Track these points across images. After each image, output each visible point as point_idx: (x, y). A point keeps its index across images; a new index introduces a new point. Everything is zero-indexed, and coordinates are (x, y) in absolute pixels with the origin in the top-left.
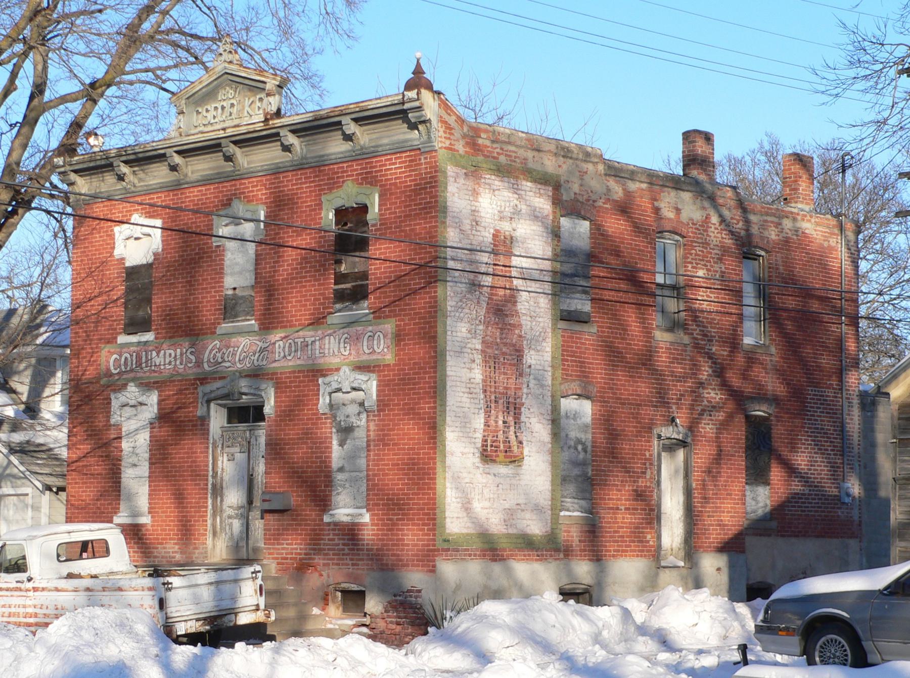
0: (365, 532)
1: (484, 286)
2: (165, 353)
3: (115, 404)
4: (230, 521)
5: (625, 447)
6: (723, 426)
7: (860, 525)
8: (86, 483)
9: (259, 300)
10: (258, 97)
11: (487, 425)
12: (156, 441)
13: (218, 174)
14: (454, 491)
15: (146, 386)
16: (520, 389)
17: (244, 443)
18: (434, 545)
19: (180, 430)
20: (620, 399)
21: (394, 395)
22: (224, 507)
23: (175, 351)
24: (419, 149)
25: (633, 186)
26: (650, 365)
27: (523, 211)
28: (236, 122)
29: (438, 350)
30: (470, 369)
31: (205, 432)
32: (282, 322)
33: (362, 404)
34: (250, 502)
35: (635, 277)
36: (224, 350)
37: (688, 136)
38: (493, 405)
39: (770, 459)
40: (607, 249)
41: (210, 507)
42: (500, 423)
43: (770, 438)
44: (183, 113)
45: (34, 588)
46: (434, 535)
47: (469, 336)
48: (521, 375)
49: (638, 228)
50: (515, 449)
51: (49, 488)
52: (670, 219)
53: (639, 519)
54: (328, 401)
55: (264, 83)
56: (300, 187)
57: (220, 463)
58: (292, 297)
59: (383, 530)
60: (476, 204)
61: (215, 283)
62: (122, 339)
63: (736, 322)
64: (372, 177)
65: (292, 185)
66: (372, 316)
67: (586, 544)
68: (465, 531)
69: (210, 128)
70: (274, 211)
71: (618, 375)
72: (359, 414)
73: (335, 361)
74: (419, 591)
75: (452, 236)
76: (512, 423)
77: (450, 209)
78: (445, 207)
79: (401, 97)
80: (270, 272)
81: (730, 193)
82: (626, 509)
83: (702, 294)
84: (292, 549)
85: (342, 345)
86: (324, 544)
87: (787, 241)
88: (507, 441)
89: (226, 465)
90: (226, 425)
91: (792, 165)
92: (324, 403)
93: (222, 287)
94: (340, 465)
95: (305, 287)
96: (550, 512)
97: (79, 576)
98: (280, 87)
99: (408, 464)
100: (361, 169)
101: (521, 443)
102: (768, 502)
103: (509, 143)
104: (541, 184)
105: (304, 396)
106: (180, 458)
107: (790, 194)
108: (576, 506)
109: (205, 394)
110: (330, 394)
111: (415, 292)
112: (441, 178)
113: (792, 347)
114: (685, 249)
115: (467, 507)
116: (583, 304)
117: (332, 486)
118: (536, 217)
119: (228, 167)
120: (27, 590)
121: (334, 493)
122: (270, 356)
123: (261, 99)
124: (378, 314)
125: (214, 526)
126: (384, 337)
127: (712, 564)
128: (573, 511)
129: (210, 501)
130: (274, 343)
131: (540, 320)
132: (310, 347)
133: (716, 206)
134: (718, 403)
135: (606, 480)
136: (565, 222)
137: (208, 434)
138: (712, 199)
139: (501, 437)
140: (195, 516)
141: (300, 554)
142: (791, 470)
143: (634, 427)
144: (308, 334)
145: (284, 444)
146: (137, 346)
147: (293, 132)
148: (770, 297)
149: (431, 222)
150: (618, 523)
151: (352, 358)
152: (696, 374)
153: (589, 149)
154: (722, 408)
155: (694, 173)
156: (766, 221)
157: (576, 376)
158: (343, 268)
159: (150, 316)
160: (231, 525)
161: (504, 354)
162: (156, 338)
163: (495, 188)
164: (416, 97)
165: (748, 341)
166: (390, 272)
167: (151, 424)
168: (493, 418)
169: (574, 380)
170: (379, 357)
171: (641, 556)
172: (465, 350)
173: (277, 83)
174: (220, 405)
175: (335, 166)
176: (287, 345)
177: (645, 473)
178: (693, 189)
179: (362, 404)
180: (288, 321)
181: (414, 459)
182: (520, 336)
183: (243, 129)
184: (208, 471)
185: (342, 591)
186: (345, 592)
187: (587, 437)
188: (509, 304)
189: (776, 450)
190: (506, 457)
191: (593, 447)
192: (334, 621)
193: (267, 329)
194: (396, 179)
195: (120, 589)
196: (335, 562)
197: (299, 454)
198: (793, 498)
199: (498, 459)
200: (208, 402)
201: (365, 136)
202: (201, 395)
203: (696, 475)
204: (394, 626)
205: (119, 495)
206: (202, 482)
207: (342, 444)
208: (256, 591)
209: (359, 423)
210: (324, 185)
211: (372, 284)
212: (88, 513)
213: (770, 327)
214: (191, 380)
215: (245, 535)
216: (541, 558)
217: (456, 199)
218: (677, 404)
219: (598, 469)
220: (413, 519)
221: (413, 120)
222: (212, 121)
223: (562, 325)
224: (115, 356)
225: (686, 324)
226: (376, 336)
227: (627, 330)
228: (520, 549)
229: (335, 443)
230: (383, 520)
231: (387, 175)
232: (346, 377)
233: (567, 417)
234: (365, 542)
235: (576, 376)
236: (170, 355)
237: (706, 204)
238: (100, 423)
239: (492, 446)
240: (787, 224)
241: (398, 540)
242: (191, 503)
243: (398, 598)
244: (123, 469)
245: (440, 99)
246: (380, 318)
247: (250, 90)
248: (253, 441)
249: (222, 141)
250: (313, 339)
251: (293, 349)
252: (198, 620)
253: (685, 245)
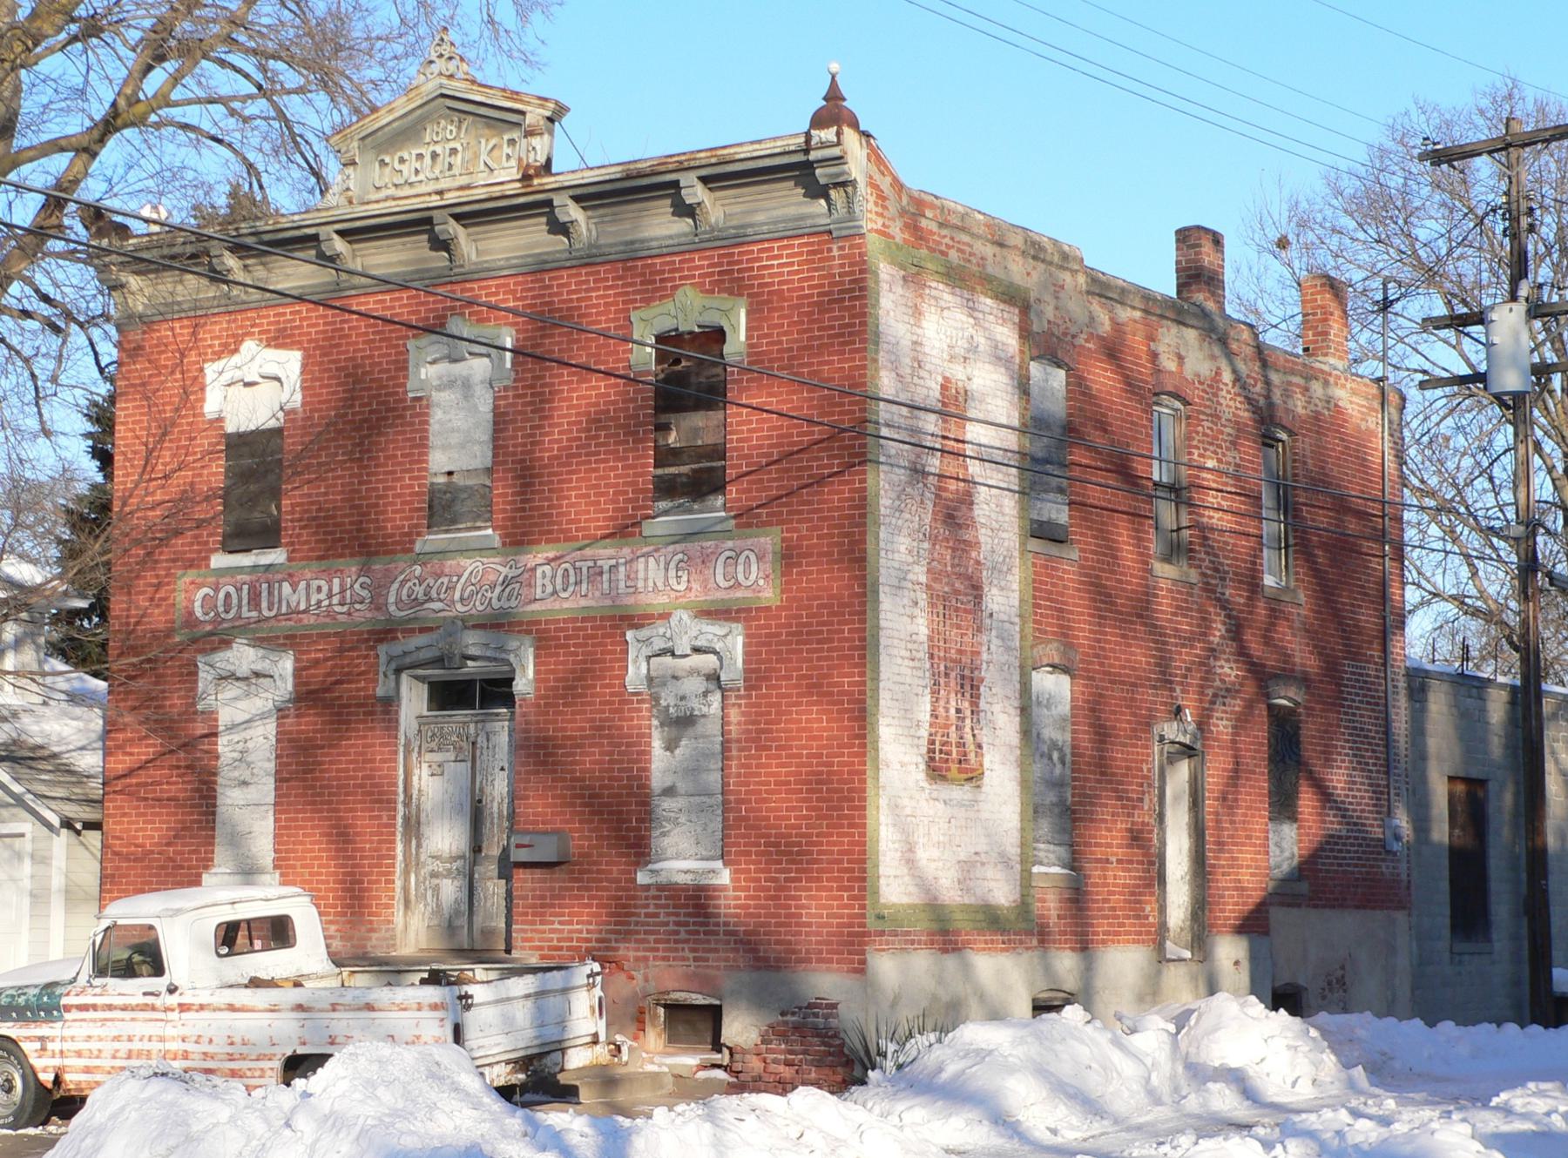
0: (722, 902)
1: (930, 474)
2: (308, 586)
3: (205, 676)
4: (435, 881)
5: (1118, 755)
6: (1241, 722)
7: (1408, 888)
8: (144, 815)
9: (503, 493)
10: (506, 137)
11: (934, 716)
12: (290, 741)
13: (417, 271)
14: (891, 829)
15: (269, 641)
16: (978, 653)
17: (464, 744)
18: (863, 925)
19: (339, 722)
20: (1109, 673)
21: (777, 661)
22: (423, 858)
23: (330, 582)
24: (830, 232)
25: (1125, 314)
26: (1148, 617)
27: (981, 348)
28: (464, 181)
29: (868, 582)
30: (912, 617)
31: (392, 723)
32: (550, 532)
33: (714, 677)
34: (476, 848)
35: (1127, 467)
36: (431, 581)
37: (1187, 237)
38: (942, 681)
39: (1297, 778)
40: (1090, 419)
41: (400, 857)
42: (953, 711)
43: (1298, 743)
44: (353, 163)
45: (180, 1005)
46: (863, 907)
47: (911, 560)
48: (979, 630)
49: (1131, 385)
50: (972, 756)
51: (67, 824)
52: (1171, 373)
53: (1135, 878)
54: (644, 671)
55: (523, 113)
56: (596, 299)
57: (415, 779)
58: (569, 489)
59: (759, 898)
60: (919, 331)
61: (411, 463)
62: (219, 560)
63: (1254, 549)
64: (732, 280)
65: (569, 293)
66: (733, 522)
67: (1064, 924)
68: (905, 900)
69: (407, 191)
70: (534, 338)
71: (1106, 634)
72: (705, 694)
73: (659, 601)
74: (834, 1006)
75: (886, 384)
76: (968, 713)
77: (883, 338)
78: (877, 334)
79: (802, 139)
80: (524, 445)
81: (1246, 335)
82: (1119, 861)
83: (1212, 499)
84: (570, 931)
85: (672, 573)
86: (637, 924)
87: (1317, 416)
88: (961, 745)
89: (428, 781)
90: (426, 713)
91: (1318, 293)
92: (638, 674)
93: (426, 469)
94: (668, 784)
95: (596, 470)
96: (1018, 867)
97: (271, 984)
98: (551, 120)
99: (808, 782)
100: (709, 266)
101: (980, 746)
102: (1296, 850)
103: (963, 229)
104: (1005, 302)
105: (594, 661)
106: (338, 770)
107: (1316, 342)
108: (1051, 856)
109: (391, 659)
110: (649, 658)
111: (820, 481)
112: (871, 284)
113: (1326, 593)
114: (1188, 425)
115: (910, 861)
116: (1058, 511)
117: (651, 821)
118: (999, 358)
119: (440, 259)
120: (167, 1009)
121: (655, 833)
122: (524, 591)
123: (512, 142)
124: (746, 518)
125: (406, 890)
126: (759, 559)
127: (1230, 951)
128: (1049, 865)
129: (399, 848)
130: (534, 569)
131: (1005, 535)
132: (605, 577)
133: (1230, 355)
134: (1234, 683)
135: (1092, 813)
136: (1035, 369)
137: (396, 729)
138: (1223, 341)
139: (953, 737)
140: (371, 873)
141: (588, 940)
142: (1325, 795)
143: (1129, 722)
144: (605, 554)
145: (555, 747)
146: (249, 574)
147: (577, 199)
148: (1295, 510)
149: (854, 360)
150: (1107, 885)
151: (692, 595)
152: (1205, 634)
153: (1066, 248)
154: (1237, 691)
155: (1199, 297)
156: (1289, 383)
157: (1054, 633)
158: (672, 438)
159: (277, 522)
160: (436, 890)
161: (956, 592)
162: (290, 559)
163: (942, 304)
165: (1269, 581)
166: (770, 446)
167: (279, 710)
168: (942, 703)
169: (1050, 641)
170: (748, 594)
171: (1138, 942)
172: (904, 584)
173: (548, 114)
174: (417, 678)
175: (658, 261)
176: (560, 572)
177: (1141, 800)
178: (1200, 325)
179: (714, 677)
180: (561, 531)
181: (821, 773)
182: (978, 563)
183: (480, 193)
184: (395, 793)
185: (665, 1006)
186: (674, 1009)
187: (1064, 738)
188: (964, 508)
189: (1307, 764)
190: (960, 771)
191: (1073, 755)
192: (657, 1059)
193: (520, 543)
194: (780, 283)
195: (370, 1007)
196: (660, 954)
197: (589, 761)
198: (1328, 843)
199: (949, 775)
200: (398, 671)
201: (717, 209)
202: (383, 659)
203: (1210, 804)
204: (781, 1068)
205: (213, 837)
206: (384, 814)
207: (670, 746)
208: (592, 1008)
209: (705, 709)
210: (634, 293)
211: (732, 466)
212: (148, 867)
213: (1296, 559)
214: (362, 633)
215: (464, 907)
216: (1010, 947)
217: (892, 322)
218: (1181, 683)
219: (1079, 791)
220: (819, 880)
221: (822, 181)
222: (413, 179)
223: (1034, 545)
224: (206, 590)
225: (1191, 550)
226: (742, 559)
227: (1116, 557)
228: (981, 932)
229: (657, 744)
230: (758, 880)
232: (687, 629)
233: (1039, 703)
234: (722, 920)
235: (1054, 633)
236: (319, 589)
237: (1217, 350)
238: (176, 702)
239: (941, 752)
240: (1317, 388)
241: (788, 916)
242: (363, 850)
243: (789, 1018)
244: (219, 790)
245: (869, 144)
246: (749, 525)
247: (489, 126)
248: (481, 740)
249: (435, 213)
250: (613, 562)
251: (572, 580)
252: (508, 1062)
253: (1188, 417)
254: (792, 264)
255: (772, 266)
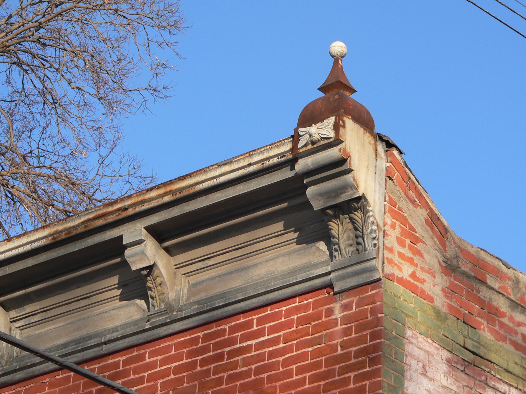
24: (330, 286)
164: (332, 134)
201: (178, 280)
221: (317, 205)
231: (235, 365)
254: (276, 341)
255: (248, 349)
